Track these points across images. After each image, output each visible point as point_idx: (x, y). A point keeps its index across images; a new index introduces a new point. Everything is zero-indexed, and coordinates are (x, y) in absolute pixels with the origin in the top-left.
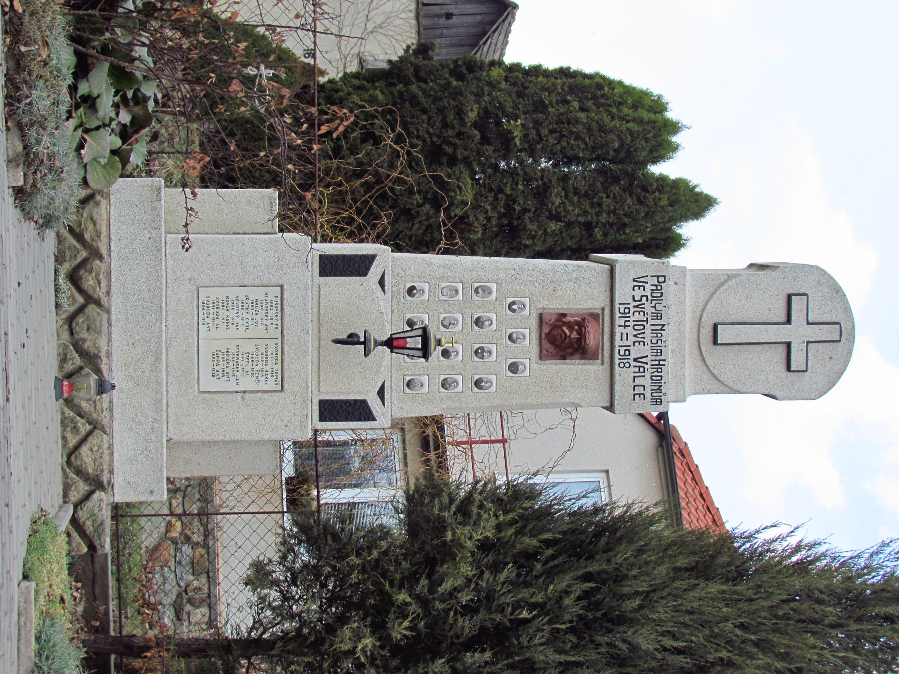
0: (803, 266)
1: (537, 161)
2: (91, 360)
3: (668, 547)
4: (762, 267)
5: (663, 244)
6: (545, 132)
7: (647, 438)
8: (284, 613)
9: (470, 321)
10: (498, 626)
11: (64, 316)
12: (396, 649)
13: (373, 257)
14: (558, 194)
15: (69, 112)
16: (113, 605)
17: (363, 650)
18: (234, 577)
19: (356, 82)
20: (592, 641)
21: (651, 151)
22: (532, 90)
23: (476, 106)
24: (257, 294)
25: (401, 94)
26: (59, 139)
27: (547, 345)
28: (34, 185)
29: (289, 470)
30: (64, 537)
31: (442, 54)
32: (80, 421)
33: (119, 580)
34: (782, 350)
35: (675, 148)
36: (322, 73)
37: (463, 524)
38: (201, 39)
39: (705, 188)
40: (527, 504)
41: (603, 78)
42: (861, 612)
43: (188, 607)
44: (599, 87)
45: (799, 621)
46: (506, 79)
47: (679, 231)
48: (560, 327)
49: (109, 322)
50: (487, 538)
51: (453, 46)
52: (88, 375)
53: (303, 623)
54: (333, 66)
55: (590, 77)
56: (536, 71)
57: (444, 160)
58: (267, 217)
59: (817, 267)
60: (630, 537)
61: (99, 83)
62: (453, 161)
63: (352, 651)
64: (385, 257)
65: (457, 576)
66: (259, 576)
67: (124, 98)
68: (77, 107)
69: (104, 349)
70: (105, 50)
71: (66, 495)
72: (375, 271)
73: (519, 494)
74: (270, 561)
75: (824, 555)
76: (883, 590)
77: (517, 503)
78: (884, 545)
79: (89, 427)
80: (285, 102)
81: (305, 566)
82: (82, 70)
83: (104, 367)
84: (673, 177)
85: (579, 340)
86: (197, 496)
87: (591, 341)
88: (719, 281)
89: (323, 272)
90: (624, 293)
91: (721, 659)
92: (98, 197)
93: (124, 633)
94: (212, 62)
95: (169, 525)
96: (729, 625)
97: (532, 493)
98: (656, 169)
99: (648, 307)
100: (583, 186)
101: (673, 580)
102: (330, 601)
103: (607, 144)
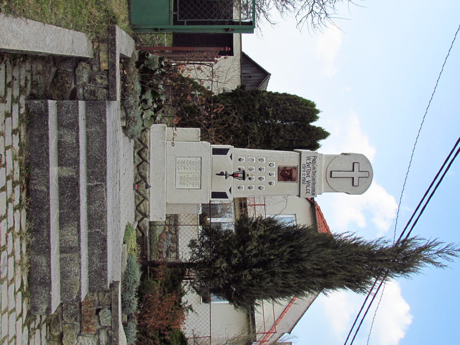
0: (358, 154)
1: (276, 121)
2: (144, 178)
3: (316, 238)
4: (346, 154)
5: (314, 146)
6: (279, 112)
7: (308, 205)
8: (199, 255)
9: (257, 169)
10: (264, 261)
11: (136, 165)
12: (233, 267)
13: (229, 149)
14: (282, 131)
15: (139, 104)
16: (149, 251)
17: (223, 267)
18: (185, 244)
19: (222, 96)
20: (292, 266)
21: (311, 118)
22: (275, 99)
23: (258, 104)
24: (193, 160)
25: (236, 100)
26: (136, 112)
27: (280, 177)
28: (129, 126)
29: (200, 213)
30: (135, 232)
31: (248, 88)
32: (140, 197)
33: (150, 244)
34: (351, 179)
35: (318, 118)
36: (213, 93)
37: (254, 230)
38: (179, 82)
39: (326, 130)
40: (273, 224)
41: (297, 96)
42: (373, 259)
43: (170, 253)
44: (295, 99)
45: (355, 261)
46: (268, 96)
47: (319, 143)
48: (284, 171)
49: (149, 167)
50: (261, 234)
51: (251, 86)
52: (143, 183)
53: (205, 259)
54: (216, 91)
55: (293, 96)
56: (277, 94)
57: (248, 120)
58: (197, 137)
59: (362, 155)
60: (304, 235)
61: (148, 96)
62: (251, 121)
63: (220, 267)
64: (232, 149)
65: (252, 245)
66: (192, 244)
67: (155, 100)
68: (141, 102)
69: (148, 175)
70: (150, 86)
71: (136, 219)
72: (229, 154)
73: (271, 221)
74: (196, 240)
75: (362, 241)
76: (380, 252)
77: (270, 223)
78: (380, 239)
79: (143, 199)
80: (204, 102)
81: (206, 241)
82: (143, 91)
83: (148, 181)
84: (317, 126)
85: (290, 175)
86: (173, 220)
87: (294, 176)
88: (333, 158)
89: (214, 153)
90: (304, 161)
91: (331, 272)
92: (147, 130)
93: (152, 260)
94: (182, 90)
95: (165, 228)
96: (333, 262)
97: (275, 222)
98: (312, 124)
99: (311, 165)
100: (289, 128)
101: (317, 248)
102: (214, 252)
103: (297, 116)
